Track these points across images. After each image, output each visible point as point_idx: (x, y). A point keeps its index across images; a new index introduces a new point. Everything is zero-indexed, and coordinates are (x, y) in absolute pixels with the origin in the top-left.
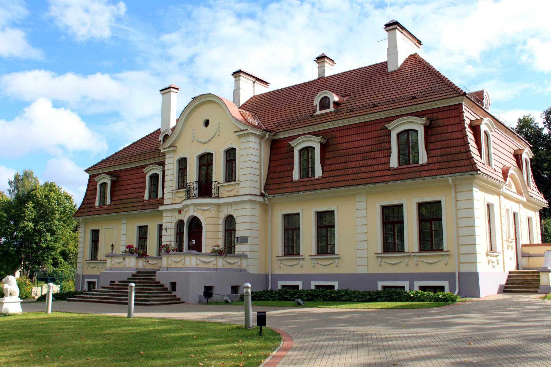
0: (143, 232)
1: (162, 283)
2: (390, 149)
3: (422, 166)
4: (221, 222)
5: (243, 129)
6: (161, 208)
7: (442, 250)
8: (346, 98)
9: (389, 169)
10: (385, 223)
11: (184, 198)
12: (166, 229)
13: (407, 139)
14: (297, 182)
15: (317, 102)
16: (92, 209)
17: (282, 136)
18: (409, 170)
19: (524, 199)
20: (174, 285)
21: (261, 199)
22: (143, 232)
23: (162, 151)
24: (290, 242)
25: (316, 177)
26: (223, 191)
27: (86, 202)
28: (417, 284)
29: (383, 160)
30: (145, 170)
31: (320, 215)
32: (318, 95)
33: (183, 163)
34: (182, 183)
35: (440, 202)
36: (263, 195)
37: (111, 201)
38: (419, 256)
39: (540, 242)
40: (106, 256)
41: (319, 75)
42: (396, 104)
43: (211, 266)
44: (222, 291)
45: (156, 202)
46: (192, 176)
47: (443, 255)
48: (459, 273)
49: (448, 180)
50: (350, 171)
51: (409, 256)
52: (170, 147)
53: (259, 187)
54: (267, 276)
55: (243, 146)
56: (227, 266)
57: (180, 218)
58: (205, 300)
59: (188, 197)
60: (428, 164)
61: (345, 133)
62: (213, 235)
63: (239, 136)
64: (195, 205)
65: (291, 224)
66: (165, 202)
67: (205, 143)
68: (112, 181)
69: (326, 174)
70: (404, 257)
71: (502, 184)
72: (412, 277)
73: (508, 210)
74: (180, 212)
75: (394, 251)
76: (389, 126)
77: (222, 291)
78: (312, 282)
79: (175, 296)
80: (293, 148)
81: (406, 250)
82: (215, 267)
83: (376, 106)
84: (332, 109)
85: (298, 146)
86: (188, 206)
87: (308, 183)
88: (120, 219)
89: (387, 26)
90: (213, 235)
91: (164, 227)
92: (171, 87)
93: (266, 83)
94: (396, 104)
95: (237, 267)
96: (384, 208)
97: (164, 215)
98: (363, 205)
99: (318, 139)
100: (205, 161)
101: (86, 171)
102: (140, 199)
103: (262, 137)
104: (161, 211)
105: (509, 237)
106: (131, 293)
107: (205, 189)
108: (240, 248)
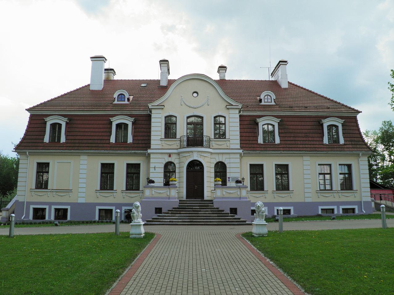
1: (220, 209)
2: (45, 131)
3: (276, 145)
6: (149, 151)
9: (323, 144)
14: (278, 145)
15: (116, 95)
16: (40, 145)
18: (121, 146)
26: (214, 144)
28: (341, 207)
29: (106, 138)
31: (129, 166)
32: (264, 92)
35: (113, 164)
42: (39, 108)
46: (182, 130)
49: (26, 153)
54: (361, 202)
60: (344, 144)
61: (291, 119)
66: (152, 147)
67: (195, 108)
69: (135, 142)
70: (139, 193)
72: (338, 204)
75: (41, 188)
76: (112, 119)
79: (239, 219)
81: (49, 188)
83: (307, 108)
87: (269, 147)
88: (79, 155)
89: (161, 61)
94: (39, 108)
96: (103, 165)
99: (66, 119)
101: (27, 110)
102: (107, 141)
104: (149, 154)
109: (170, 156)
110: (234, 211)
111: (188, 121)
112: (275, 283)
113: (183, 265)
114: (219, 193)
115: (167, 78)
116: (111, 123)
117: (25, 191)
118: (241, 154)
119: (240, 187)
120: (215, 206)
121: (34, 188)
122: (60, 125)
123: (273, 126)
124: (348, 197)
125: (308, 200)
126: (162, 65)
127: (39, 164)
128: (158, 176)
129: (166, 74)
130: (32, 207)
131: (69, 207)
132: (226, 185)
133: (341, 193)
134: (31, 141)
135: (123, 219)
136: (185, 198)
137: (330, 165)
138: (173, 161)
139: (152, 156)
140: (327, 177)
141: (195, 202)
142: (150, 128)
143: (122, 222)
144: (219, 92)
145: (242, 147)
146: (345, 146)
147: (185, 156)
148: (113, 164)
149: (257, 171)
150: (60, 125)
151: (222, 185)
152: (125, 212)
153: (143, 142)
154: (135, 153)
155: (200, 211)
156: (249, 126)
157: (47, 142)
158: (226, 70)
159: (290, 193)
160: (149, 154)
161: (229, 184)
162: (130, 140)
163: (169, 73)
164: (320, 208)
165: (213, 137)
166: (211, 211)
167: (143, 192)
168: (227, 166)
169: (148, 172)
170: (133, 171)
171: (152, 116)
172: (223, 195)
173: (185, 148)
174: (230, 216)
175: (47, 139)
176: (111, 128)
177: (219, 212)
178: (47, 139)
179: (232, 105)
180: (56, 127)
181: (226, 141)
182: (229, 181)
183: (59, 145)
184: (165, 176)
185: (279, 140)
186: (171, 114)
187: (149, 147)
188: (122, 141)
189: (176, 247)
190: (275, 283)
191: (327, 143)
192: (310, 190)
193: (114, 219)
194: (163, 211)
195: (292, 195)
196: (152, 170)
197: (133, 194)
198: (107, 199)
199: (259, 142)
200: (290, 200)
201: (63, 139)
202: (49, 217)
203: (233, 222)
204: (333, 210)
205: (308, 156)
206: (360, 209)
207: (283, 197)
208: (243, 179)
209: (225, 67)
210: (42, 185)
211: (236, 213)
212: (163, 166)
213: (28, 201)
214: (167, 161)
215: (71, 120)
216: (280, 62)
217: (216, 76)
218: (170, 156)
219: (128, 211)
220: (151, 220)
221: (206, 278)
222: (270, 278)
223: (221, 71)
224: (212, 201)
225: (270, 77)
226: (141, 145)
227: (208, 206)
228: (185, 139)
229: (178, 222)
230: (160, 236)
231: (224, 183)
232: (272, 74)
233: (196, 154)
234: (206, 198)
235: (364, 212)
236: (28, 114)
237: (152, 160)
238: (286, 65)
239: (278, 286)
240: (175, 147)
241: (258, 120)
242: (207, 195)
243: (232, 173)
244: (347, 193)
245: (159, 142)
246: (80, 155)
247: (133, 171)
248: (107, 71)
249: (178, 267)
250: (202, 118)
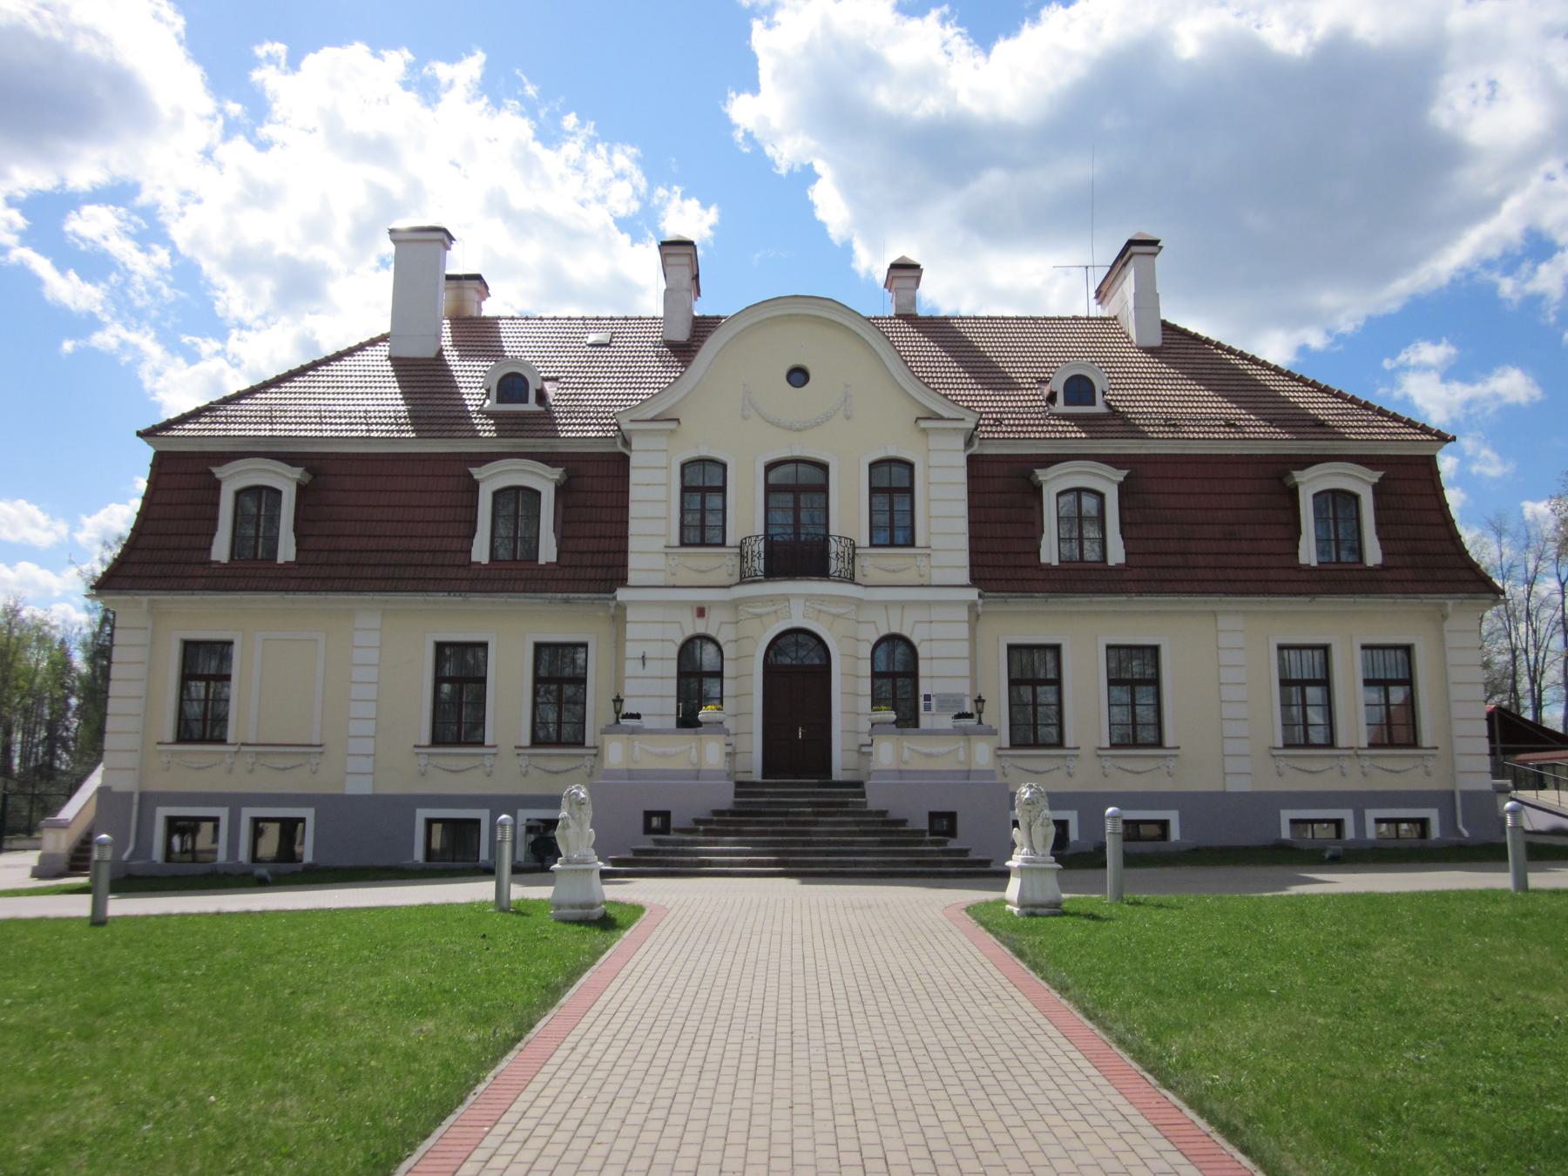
1: (893, 815)
3: (1370, 569)
6: (622, 594)
7: (481, 744)
9: (1040, 567)
10: (187, 676)
18: (515, 574)
37: (300, 549)
38: (1372, 757)
46: (746, 513)
47: (583, 756)
48: (143, 795)
52: (652, 420)
54: (1452, 793)
64: (808, 597)
66: (633, 578)
67: (798, 430)
70: (583, 756)
72: (1359, 801)
78: (419, 811)
79: (965, 852)
87: (1082, 579)
109: (701, 612)
110: (944, 823)
111: (772, 480)
112: (1063, 1060)
113: (742, 1004)
114: (889, 753)
115: (690, 310)
116: (474, 487)
117: (136, 749)
118: (972, 606)
119: (966, 732)
120: (874, 801)
121: (1364, 744)
123: (1101, 496)
124: (1398, 773)
125: (1236, 785)
126: (670, 260)
127: (191, 649)
128: (654, 691)
129: (687, 295)
130: (162, 813)
131: (308, 813)
132: (915, 723)
133: (1372, 757)
134: (156, 557)
135: (520, 857)
136: (757, 775)
137: (1326, 649)
138: (712, 632)
139: (631, 615)
140: (1314, 693)
141: (797, 793)
142: (624, 507)
143: (517, 870)
144: (892, 370)
145: (976, 580)
146: (1388, 575)
147: (759, 616)
148: (230, 643)
149: (1034, 672)
151: (897, 723)
152: (530, 829)
153: (596, 561)
155: (816, 823)
156: (1003, 493)
157: (292, 558)
158: (918, 279)
159: (1165, 757)
160: (622, 607)
161: (925, 720)
162: (548, 551)
163: (698, 293)
164: (1286, 815)
165: (864, 540)
166: (858, 823)
167: (598, 752)
168: (922, 651)
169: (619, 676)
170: (559, 674)
171: (633, 462)
172: (906, 763)
173: (759, 581)
174: (931, 847)
176: (474, 506)
177: (888, 828)
179: (941, 418)
181: (915, 555)
182: (928, 708)
184: (683, 694)
185: (1379, 552)
186: (704, 452)
187: (623, 581)
188: (256, 554)
189: (721, 947)
190: (1063, 1060)
191: (1314, 563)
193: (484, 854)
194: (675, 822)
195: (1172, 763)
196: (632, 667)
197: (556, 759)
198: (459, 776)
199: (1044, 559)
200: (1167, 785)
202: (228, 854)
203: (940, 863)
204: (1164, 824)
205: (1237, 612)
206: (1449, 822)
207: (1139, 773)
208: (979, 700)
209: (916, 267)
210: (201, 723)
211: (952, 832)
212: (673, 652)
214: (689, 632)
216: (1131, 243)
217: (884, 306)
218: (701, 612)
219: (538, 828)
220: (630, 856)
221: (821, 1043)
222: (1049, 1044)
223: (896, 283)
224: (859, 784)
225: (1093, 302)
226: (590, 573)
227: (846, 804)
228: (760, 547)
229: (731, 864)
230: (665, 911)
231: (908, 720)
232: (1098, 293)
233: (800, 603)
234: (838, 772)
235: (1466, 833)
237: (632, 631)
238: (1155, 254)
239: (1070, 1068)
240: (720, 577)
241: (1041, 475)
242: (841, 762)
243: (941, 674)
244: (1395, 759)
245: (660, 561)
247: (559, 674)
248: (453, 283)
249: (726, 1009)
250: (823, 467)
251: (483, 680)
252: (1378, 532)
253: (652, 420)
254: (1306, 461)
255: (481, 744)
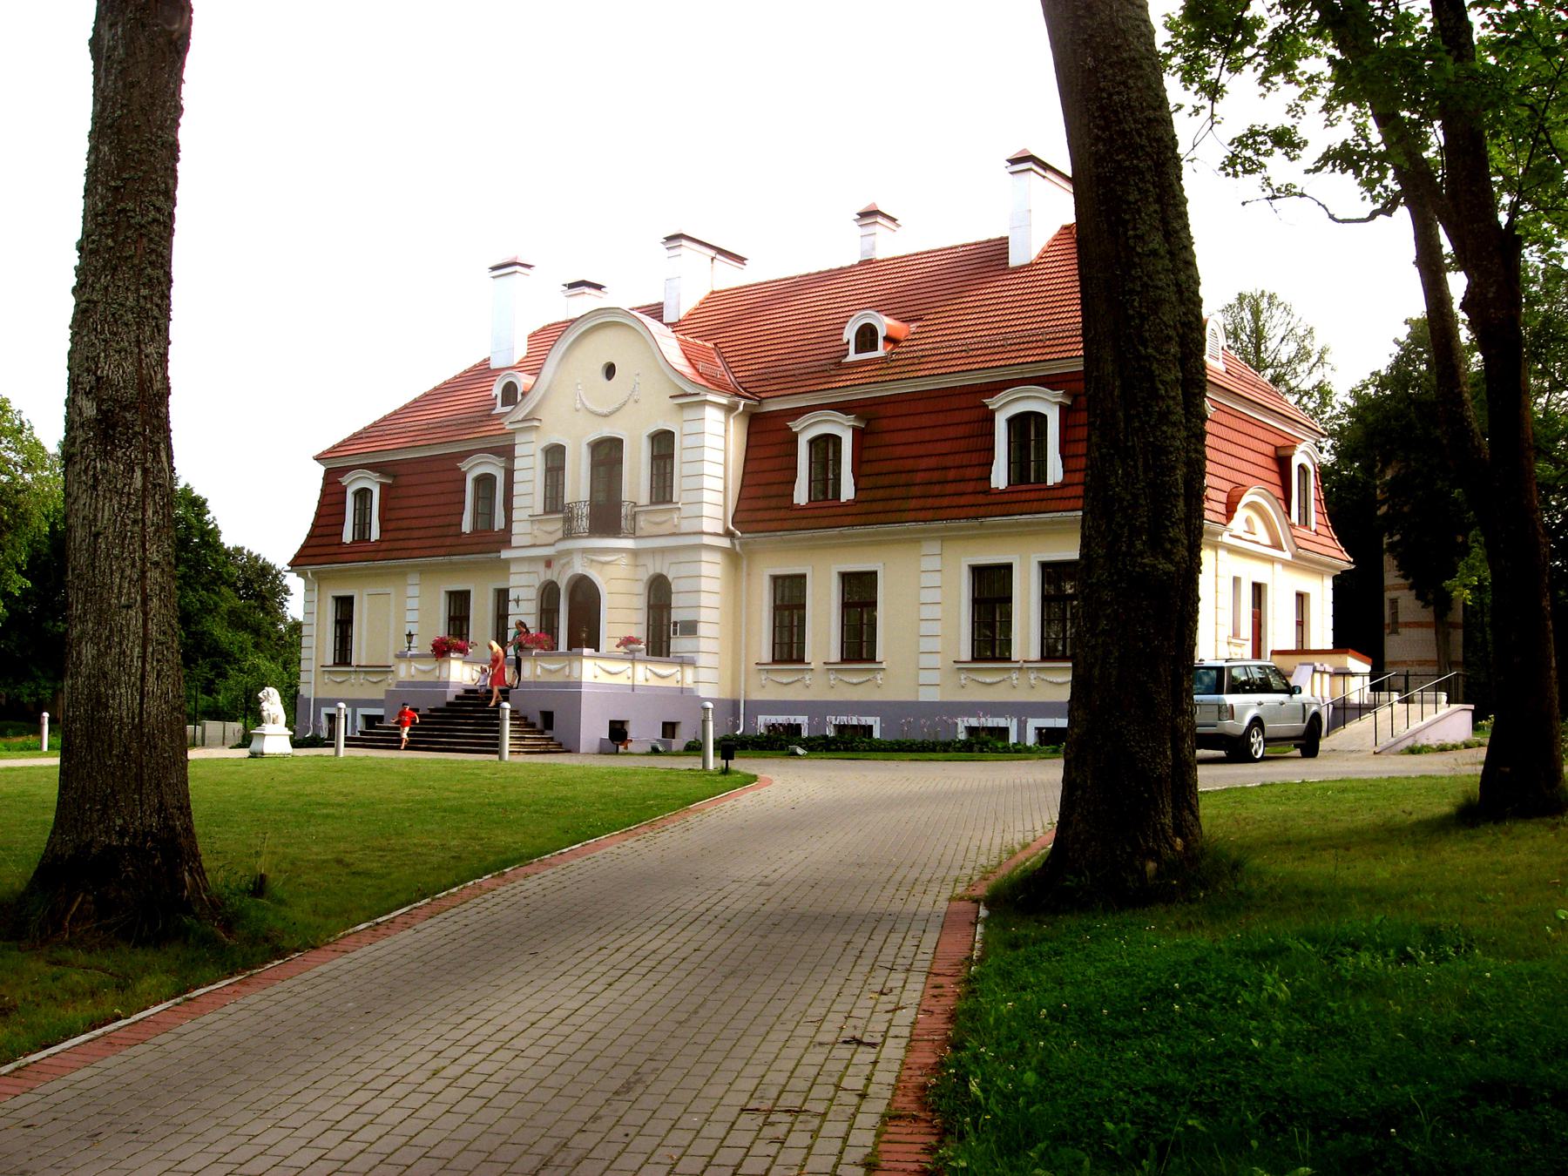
0: (459, 604)
4: (641, 588)
5: (690, 391)
6: (505, 554)
7: (1009, 660)
8: (913, 327)
11: (560, 534)
12: (517, 601)
13: (1027, 428)
14: (802, 508)
15: (849, 334)
17: (772, 406)
19: (1287, 556)
20: (548, 717)
21: (725, 543)
22: (459, 604)
23: (509, 427)
24: (786, 634)
25: (843, 499)
27: (318, 532)
28: (1033, 724)
30: (464, 466)
33: (555, 456)
34: (554, 500)
36: (728, 534)
37: (1066, 471)
39: (1330, 647)
40: (397, 656)
41: (863, 253)
43: (622, 680)
44: (643, 733)
45: (491, 541)
46: (578, 484)
50: (916, 491)
51: (1020, 669)
52: (523, 421)
53: (721, 516)
54: (736, 703)
55: (688, 428)
56: (654, 682)
57: (549, 577)
58: (613, 747)
59: (569, 534)
62: (621, 613)
63: (681, 406)
65: (789, 600)
66: (515, 541)
68: (382, 485)
71: (1219, 527)
72: (1023, 711)
73: (1236, 580)
74: (548, 563)
77: (643, 733)
80: (796, 435)
82: (629, 682)
84: (881, 352)
85: (807, 432)
86: (569, 552)
87: (827, 512)
88: (402, 573)
90: (621, 613)
91: (512, 596)
92: (514, 264)
93: (741, 260)
95: (674, 684)
96: (846, 578)
97: (513, 569)
98: (935, 563)
99: (850, 420)
100: (607, 454)
101: (317, 459)
102: (452, 531)
103: (729, 409)
104: (507, 562)
105: (1236, 634)
106: (503, 719)
107: (607, 516)
108: (679, 644)
121: (969, 658)
122: (836, 440)
148: (875, 573)
150: (1041, 419)
154: (1053, 522)
157: (851, 496)
175: (999, 477)
176: (991, 434)
178: (999, 477)
180: (1027, 428)
183: (1041, 495)
192: (935, 661)
201: (847, 491)
204: (1005, 731)
213: (320, 696)
215: (873, 419)
236: (319, 470)
244: (787, 673)
245: (528, 525)
246: (918, 541)
251: (804, 607)
252: (853, 471)
253: (523, 421)
254: (797, 413)
255: (1009, 660)
